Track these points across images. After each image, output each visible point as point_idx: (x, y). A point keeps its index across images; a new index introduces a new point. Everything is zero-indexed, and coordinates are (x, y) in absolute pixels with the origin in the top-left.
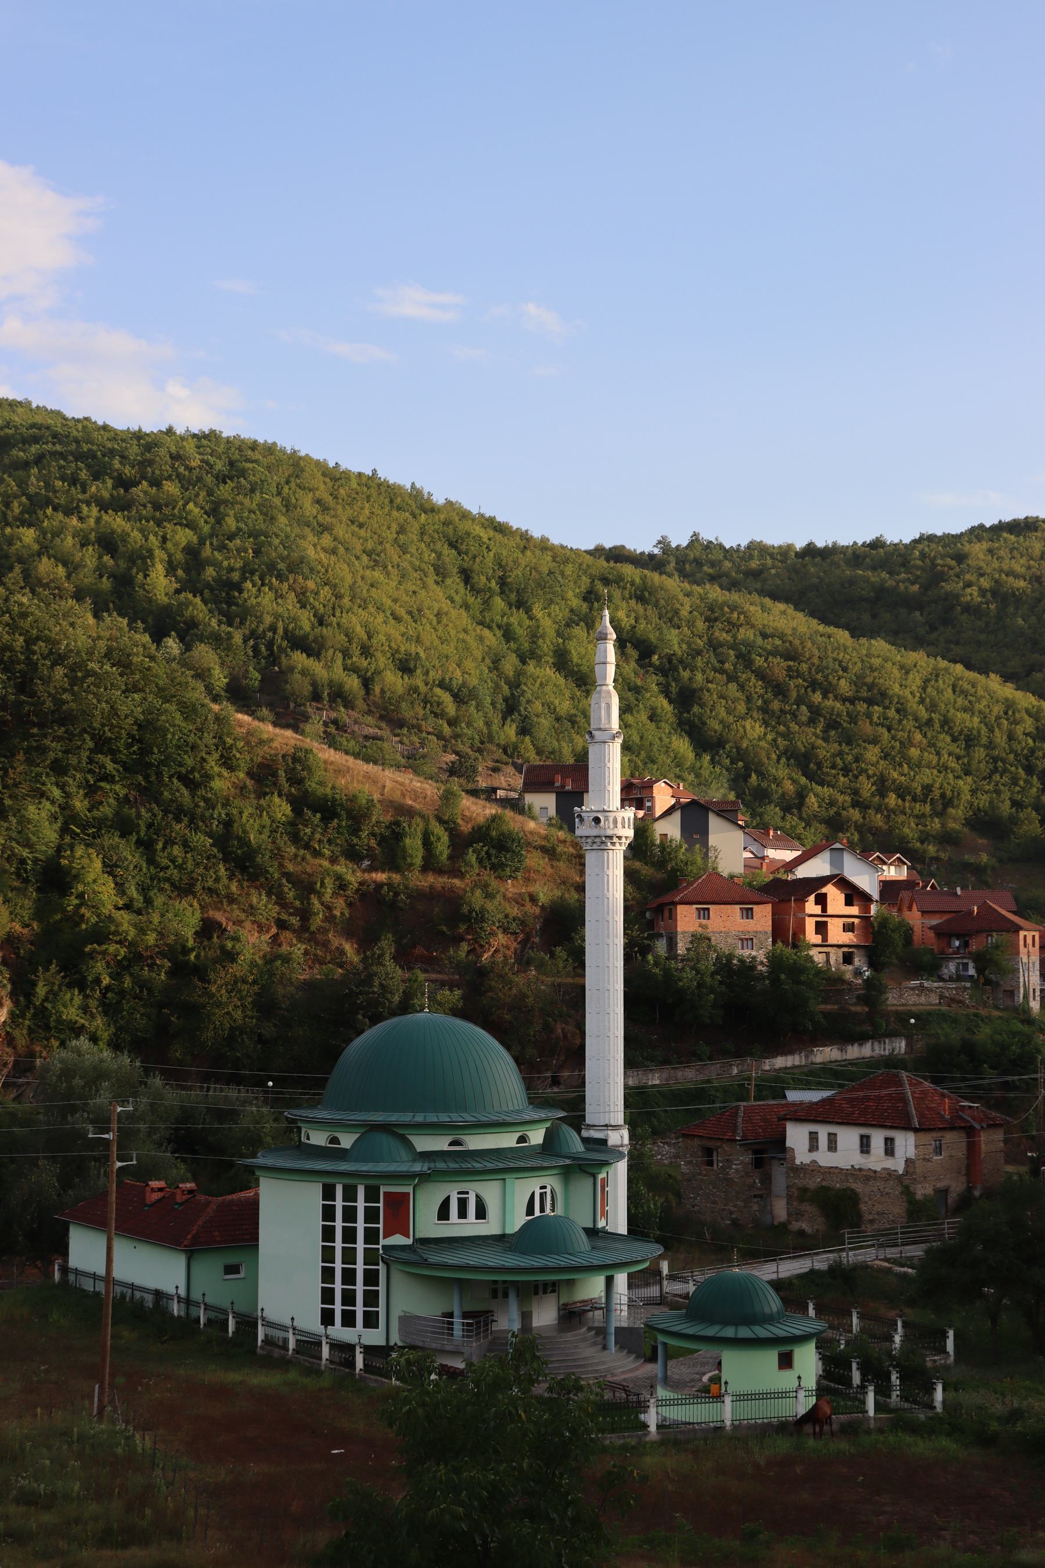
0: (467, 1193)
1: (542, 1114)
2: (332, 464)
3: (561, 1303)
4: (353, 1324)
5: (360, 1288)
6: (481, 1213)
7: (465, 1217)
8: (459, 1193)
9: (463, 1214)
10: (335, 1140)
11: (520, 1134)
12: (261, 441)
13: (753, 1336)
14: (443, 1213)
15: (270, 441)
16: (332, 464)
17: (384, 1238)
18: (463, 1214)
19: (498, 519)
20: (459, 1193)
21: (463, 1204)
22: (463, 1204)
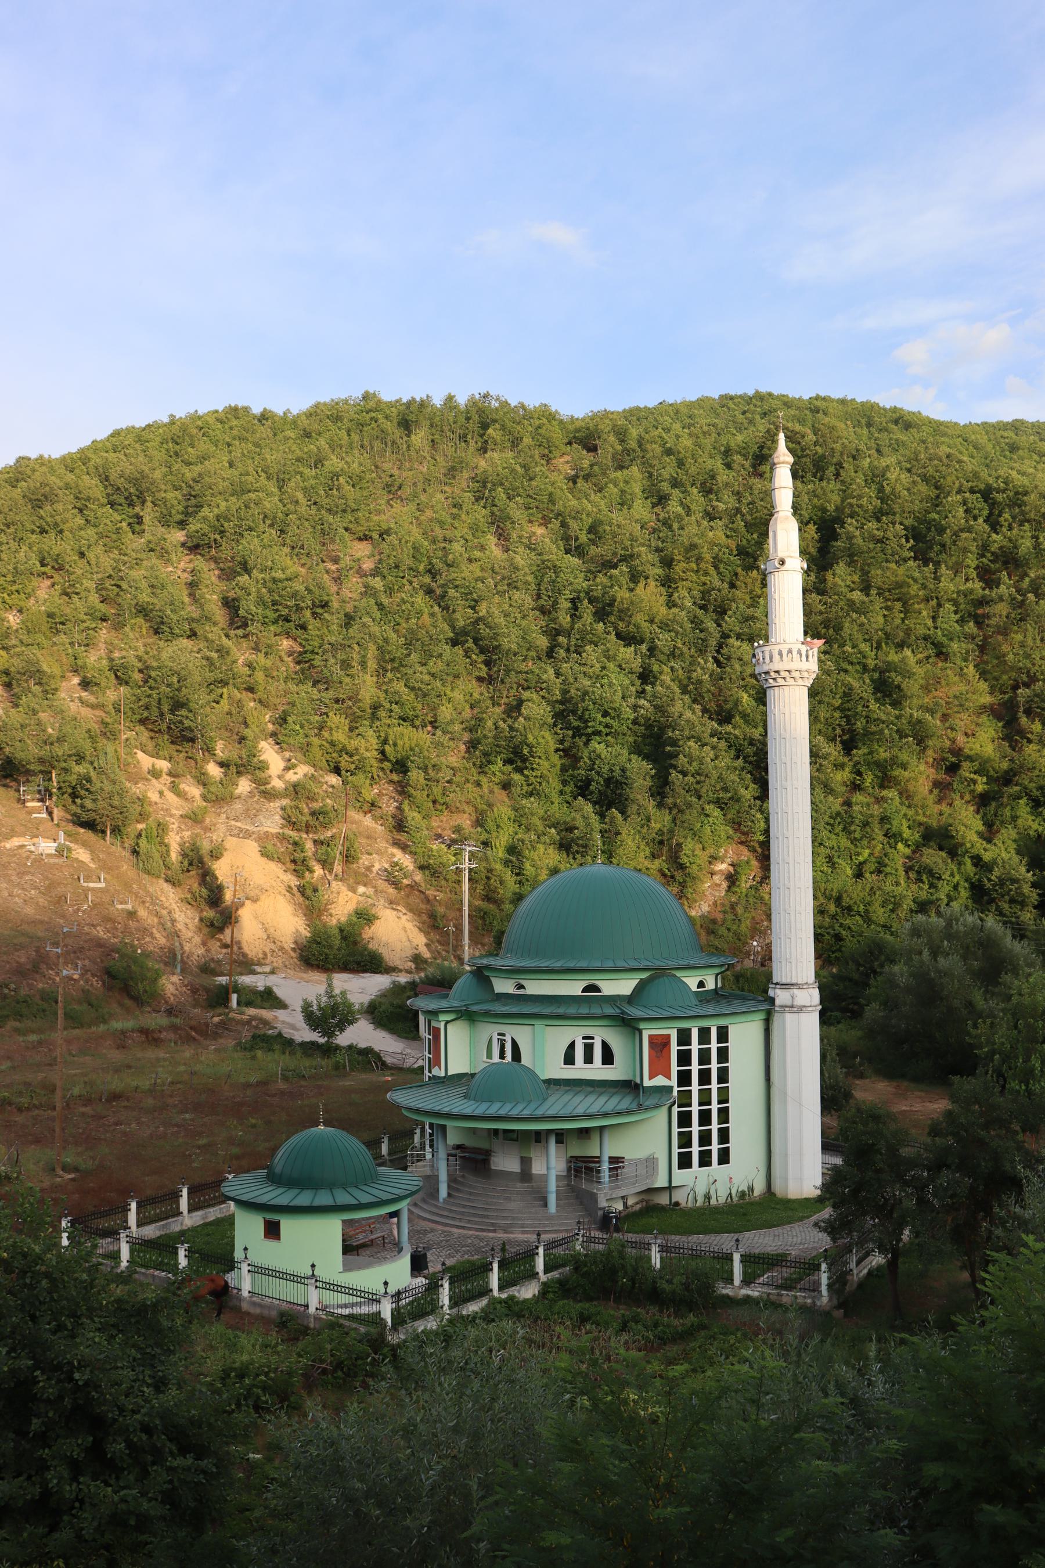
0: (593, 1038)
1: (711, 961)
2: (438, 401)
3: (569, 1155)
4: (709, 1164)
5: (695, 1129)
6: (608, 1058)
7: (573, 1063)
8: (584, 1038)
9: (589, 1059)
10: (521, 987)
11: (700, 978)
12: (240, 405)
13: (355, 1202)
14: (569, 1059)
15: (192, 411)
16: (438, 401)
17: (651, 1078)
18: (589, 1059)
19: (859, 400)
20: (584, 1038)
21: (589, 1049)
22: (589, 1049)
